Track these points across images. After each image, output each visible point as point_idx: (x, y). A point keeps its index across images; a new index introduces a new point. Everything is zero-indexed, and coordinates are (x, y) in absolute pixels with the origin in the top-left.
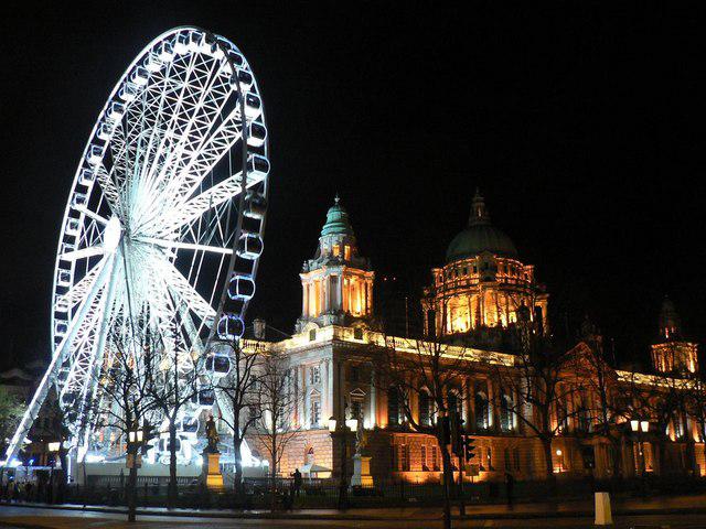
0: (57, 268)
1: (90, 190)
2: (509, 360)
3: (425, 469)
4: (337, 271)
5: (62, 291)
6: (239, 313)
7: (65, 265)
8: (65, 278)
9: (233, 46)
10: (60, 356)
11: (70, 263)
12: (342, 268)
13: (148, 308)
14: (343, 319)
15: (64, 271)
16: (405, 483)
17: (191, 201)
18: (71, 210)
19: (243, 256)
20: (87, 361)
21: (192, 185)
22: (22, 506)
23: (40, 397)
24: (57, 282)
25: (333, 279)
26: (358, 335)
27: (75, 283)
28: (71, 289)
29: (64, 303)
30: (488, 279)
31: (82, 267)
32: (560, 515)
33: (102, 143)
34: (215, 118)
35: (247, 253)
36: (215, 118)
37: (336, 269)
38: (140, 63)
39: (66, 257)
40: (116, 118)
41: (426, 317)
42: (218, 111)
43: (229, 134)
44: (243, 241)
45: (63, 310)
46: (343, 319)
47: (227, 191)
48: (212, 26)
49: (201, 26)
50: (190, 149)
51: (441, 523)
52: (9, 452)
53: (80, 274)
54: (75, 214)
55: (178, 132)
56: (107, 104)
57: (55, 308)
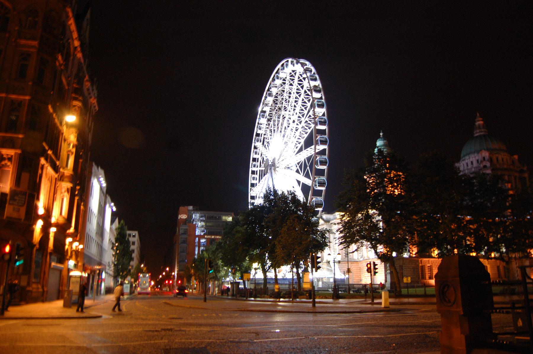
2: (255, 341)
5: (253, 185)
6: (324, 175)
7: (253, 172)
9: (307, 63)
17: (296, 155)
19: (318, 168)
21: (299, 143)
22: (358, 284)
24: (251, 181)
32: (206, 325)
33: (265, 112)
35: (320, 166)
38: (277, 72)
40: (270, 100)
44: (317, 161)
47: (310, 152)
48: (297, 55)
49: (294, 57)
51: (311, 304)
53: (261, 177)
55: (291, 85)
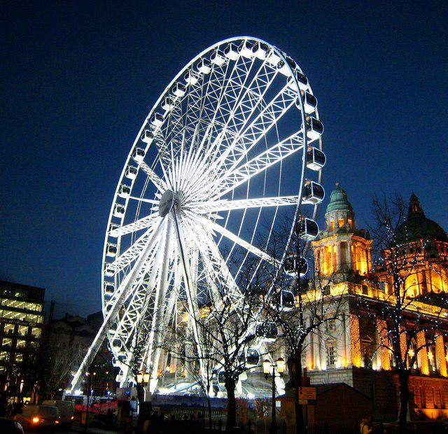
0: (106, 242)
1: (133, 182)
3: (436, 407)
4: (346, 238)
5: (110, 260)
8: (113, 250)
10: (109, 321)
11: (117, 238)
12: (351, 235)
13: (173, 276)
14: (353, 277)
15: (120, 205)
16: (424, 416)
18: (113, 217)
20: (226, 162)
23: (95, 347)
24: (106, 254)
25: (343, 245)
26: (365, 291)
27: (121, 253)
28: (117, 259)
29: (112, 269)
30: (433, 256)
31: (127, 241)
34: (129, 308)
36: (129, 308)
37: (345, 236)
39: (114, 234)
41: (84, 361)
42: (131, 303)
43: (137, 306)
45: (111, 275)
46: (353, 277)
50: (144, 285)
52: (74, 382)
54: (121, 201)
56: (151, 113)
57: (104, 273)
